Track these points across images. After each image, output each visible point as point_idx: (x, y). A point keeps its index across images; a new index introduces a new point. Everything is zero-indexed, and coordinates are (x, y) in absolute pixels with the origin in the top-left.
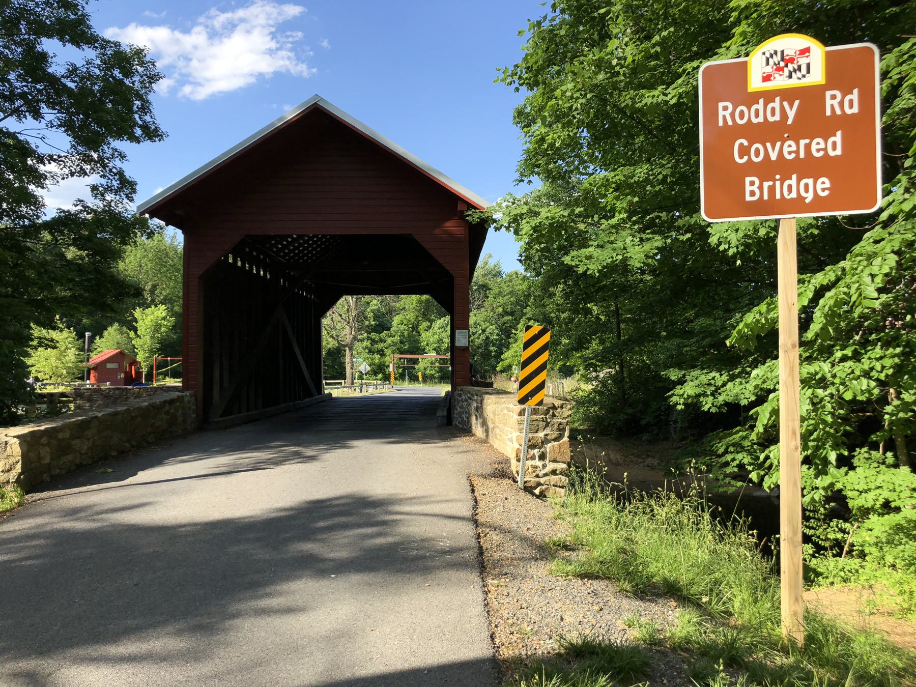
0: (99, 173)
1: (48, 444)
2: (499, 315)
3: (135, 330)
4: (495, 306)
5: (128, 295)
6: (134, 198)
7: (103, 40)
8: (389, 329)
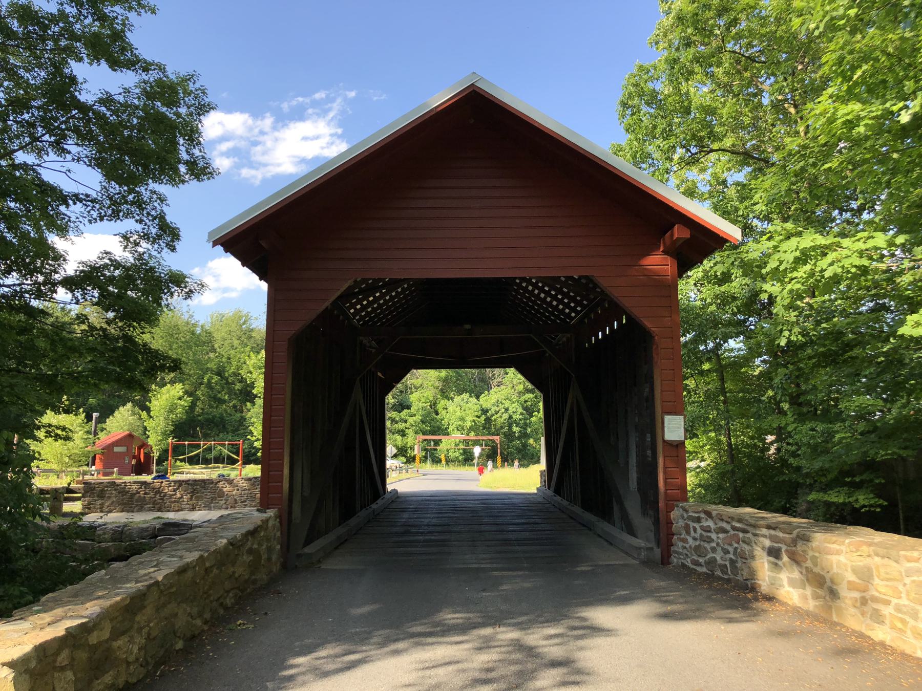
0: (134, 217)
1: (71, 666)
2: (519, 393)
3: (148, 410)
4: (515, 383)
5: (162, 368)
6: (177, 247)
7: (145, 62)
8: (409, 407)
